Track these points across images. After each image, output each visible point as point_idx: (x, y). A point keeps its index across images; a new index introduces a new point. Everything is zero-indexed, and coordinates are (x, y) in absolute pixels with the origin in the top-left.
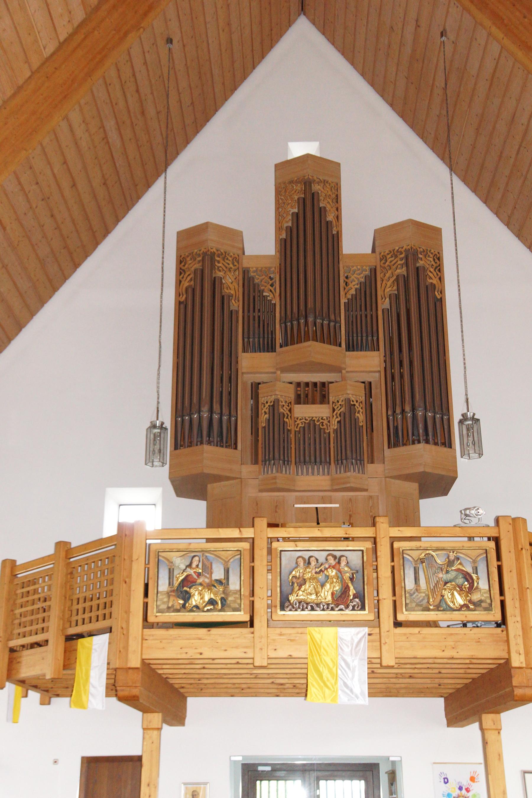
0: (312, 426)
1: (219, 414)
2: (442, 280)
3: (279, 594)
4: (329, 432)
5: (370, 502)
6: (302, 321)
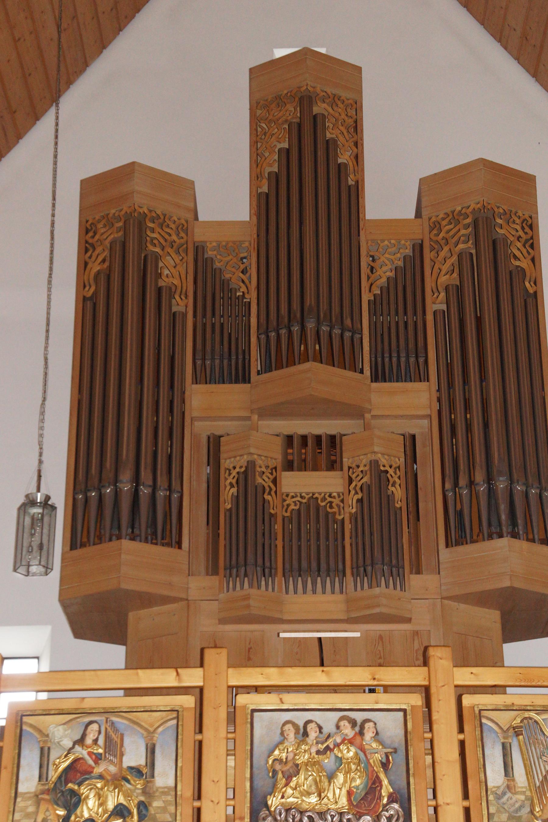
0: (313, 509)
1: (150, 486)
2: (537, 264)
3: (248, 794)
4: (343, 519)
5: (416, 642)
6: (296, 329)
